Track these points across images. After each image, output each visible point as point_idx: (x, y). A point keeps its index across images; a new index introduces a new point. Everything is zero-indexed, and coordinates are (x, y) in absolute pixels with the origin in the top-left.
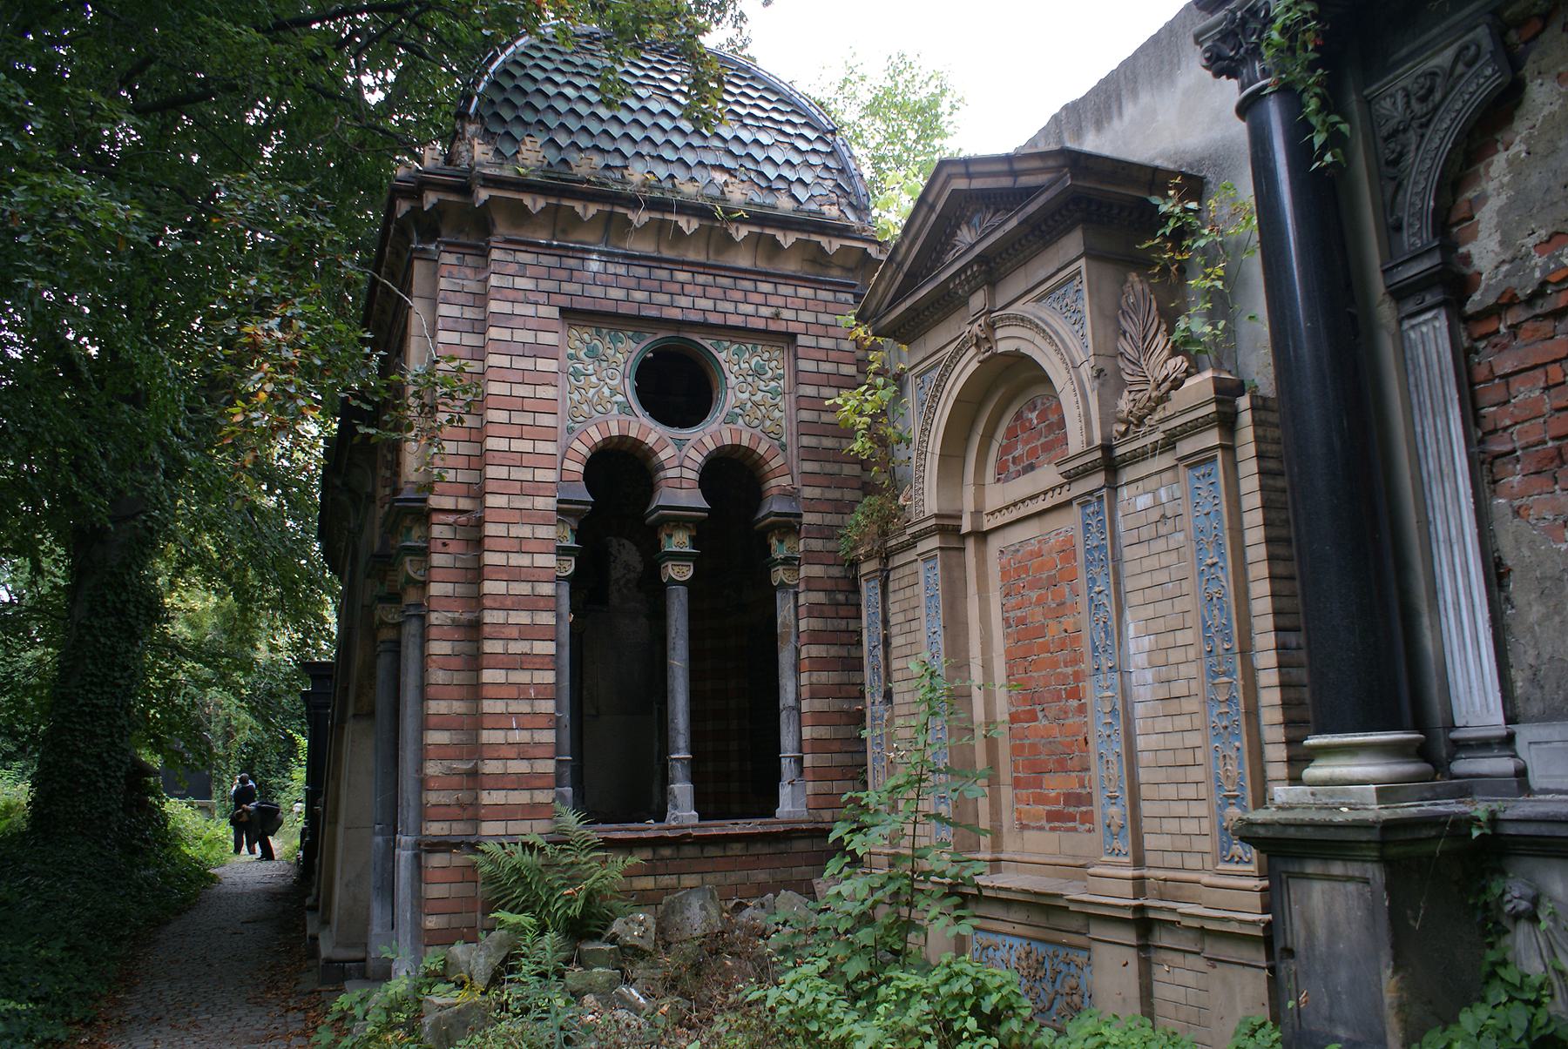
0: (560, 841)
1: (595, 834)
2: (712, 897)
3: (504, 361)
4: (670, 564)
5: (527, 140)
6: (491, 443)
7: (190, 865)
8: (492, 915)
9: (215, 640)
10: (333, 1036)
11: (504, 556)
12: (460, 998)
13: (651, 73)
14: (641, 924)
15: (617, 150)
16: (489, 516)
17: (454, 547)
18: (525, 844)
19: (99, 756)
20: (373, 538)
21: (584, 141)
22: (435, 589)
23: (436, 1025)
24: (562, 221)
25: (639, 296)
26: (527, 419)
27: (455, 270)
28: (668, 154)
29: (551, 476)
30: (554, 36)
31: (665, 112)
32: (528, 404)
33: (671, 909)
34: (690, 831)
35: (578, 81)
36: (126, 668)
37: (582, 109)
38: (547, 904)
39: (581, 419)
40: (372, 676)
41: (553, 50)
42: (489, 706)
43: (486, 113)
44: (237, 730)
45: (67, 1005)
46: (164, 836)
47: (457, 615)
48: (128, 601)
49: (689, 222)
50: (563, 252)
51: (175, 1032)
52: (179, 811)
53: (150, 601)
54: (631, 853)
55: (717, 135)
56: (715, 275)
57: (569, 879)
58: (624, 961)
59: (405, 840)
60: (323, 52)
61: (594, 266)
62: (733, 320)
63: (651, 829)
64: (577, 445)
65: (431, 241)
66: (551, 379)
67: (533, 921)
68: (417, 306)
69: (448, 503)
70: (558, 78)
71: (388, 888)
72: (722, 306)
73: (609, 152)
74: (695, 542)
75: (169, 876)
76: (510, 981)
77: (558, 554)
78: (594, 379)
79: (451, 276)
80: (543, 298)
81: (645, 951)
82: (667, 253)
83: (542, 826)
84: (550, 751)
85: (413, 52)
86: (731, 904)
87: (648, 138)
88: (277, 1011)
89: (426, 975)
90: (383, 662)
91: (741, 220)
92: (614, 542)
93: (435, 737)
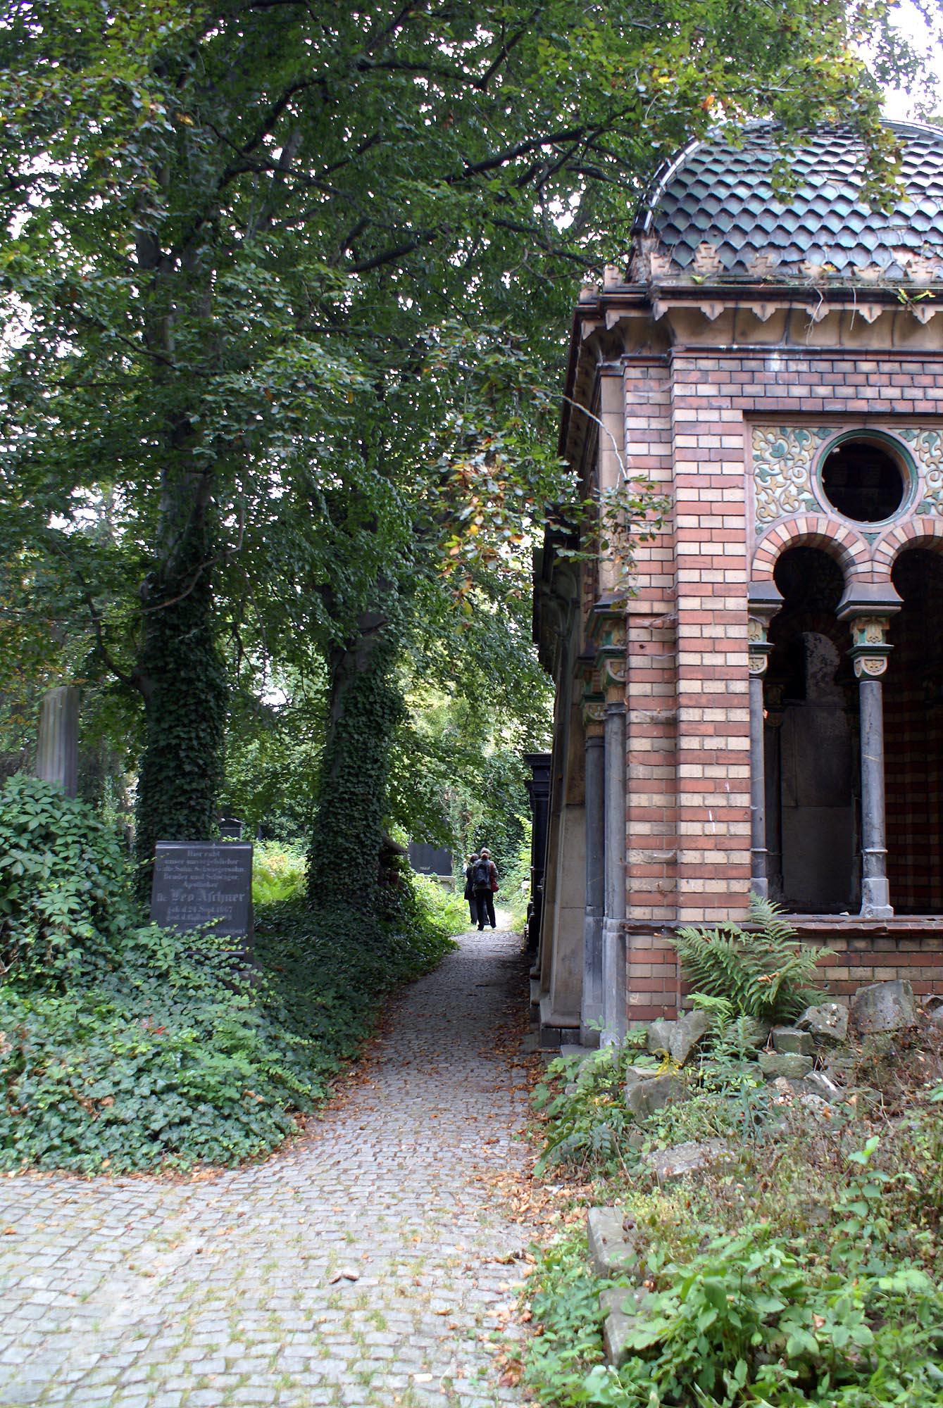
0: (756, 930)
1: (790, 923)
2: (907, 992)
3: (691, 468)
4: (862, 659)
5: (702, 247)
6: (682, 548)
7: (434, 933)
8: (690, 997)
9: (450, 735)
10: (548, 1094)
11: (698, 655)
12: (659, 1070)
13: (825, 158)
14: (833, 1013)
15: (794, 245)
16: (682, 617)
17: (651, 649)
18: (721, 931)
19: (357, 836)
20: (579, 642)
21: (759, 240)
22: (634, 689)
23: (637, 1093)
24: (739, 323)
25: (822, 391)
26: (716, 522)
27: (640, 384)
28: (847, 241)
29: (742, 576)
30: (724, 137)
31: (841, 198)
32: (716, 508)
33: (864, 1002)
34: (885, 925)
35: (750, 179)
36: (376, 761)
37: (756, 207)
38: (742, 988)
39: (769, 519)
40: (582, 768)
41: (724, 151)
42: (686, 800)
43: (660, 226)
44: (472, 815)
45: (338, 1044)
46: (412, 908)
47: (655, 713)
48: (375, 702)
49: (870, 310)
50: (744, 354)
51: (420, 1076)
52: (424, 885)
53: (393, 702)
54: (825, 944)
55: (898, 213)
56: (901, 362)
57: (764, 966)
58: (816, 1048)
59: (611, 922)
60: (507, 193)
61: (775, 365)
62: (922, 407)
63: (845, 921)
64: (766, 545)
65: (616, 358)
66: (737, 481)
67: (729, 1004)
68: (606, 424)
69: (644, 607)
70: (730, 180)
71: (596, 965)
72: (910, 393)
73: (784, 248)
74: (888, 636)
75: (417, 942)
76: (705, 1059)
77: (750, 653)
78: (780, 478)
79: (636, 389)
80: (726, 403)
81: (837, 1040)
82: (850, 345)
83: (738, 914)
84: (747, 842)
85: (592, 175)
86: (927, 1000)
87: (824, 228)
88: (503, 1066)
89: (630, 1047)
90: (591, 756)
91: (927, 301)
92: (810, 636)
93: (637, 828)
